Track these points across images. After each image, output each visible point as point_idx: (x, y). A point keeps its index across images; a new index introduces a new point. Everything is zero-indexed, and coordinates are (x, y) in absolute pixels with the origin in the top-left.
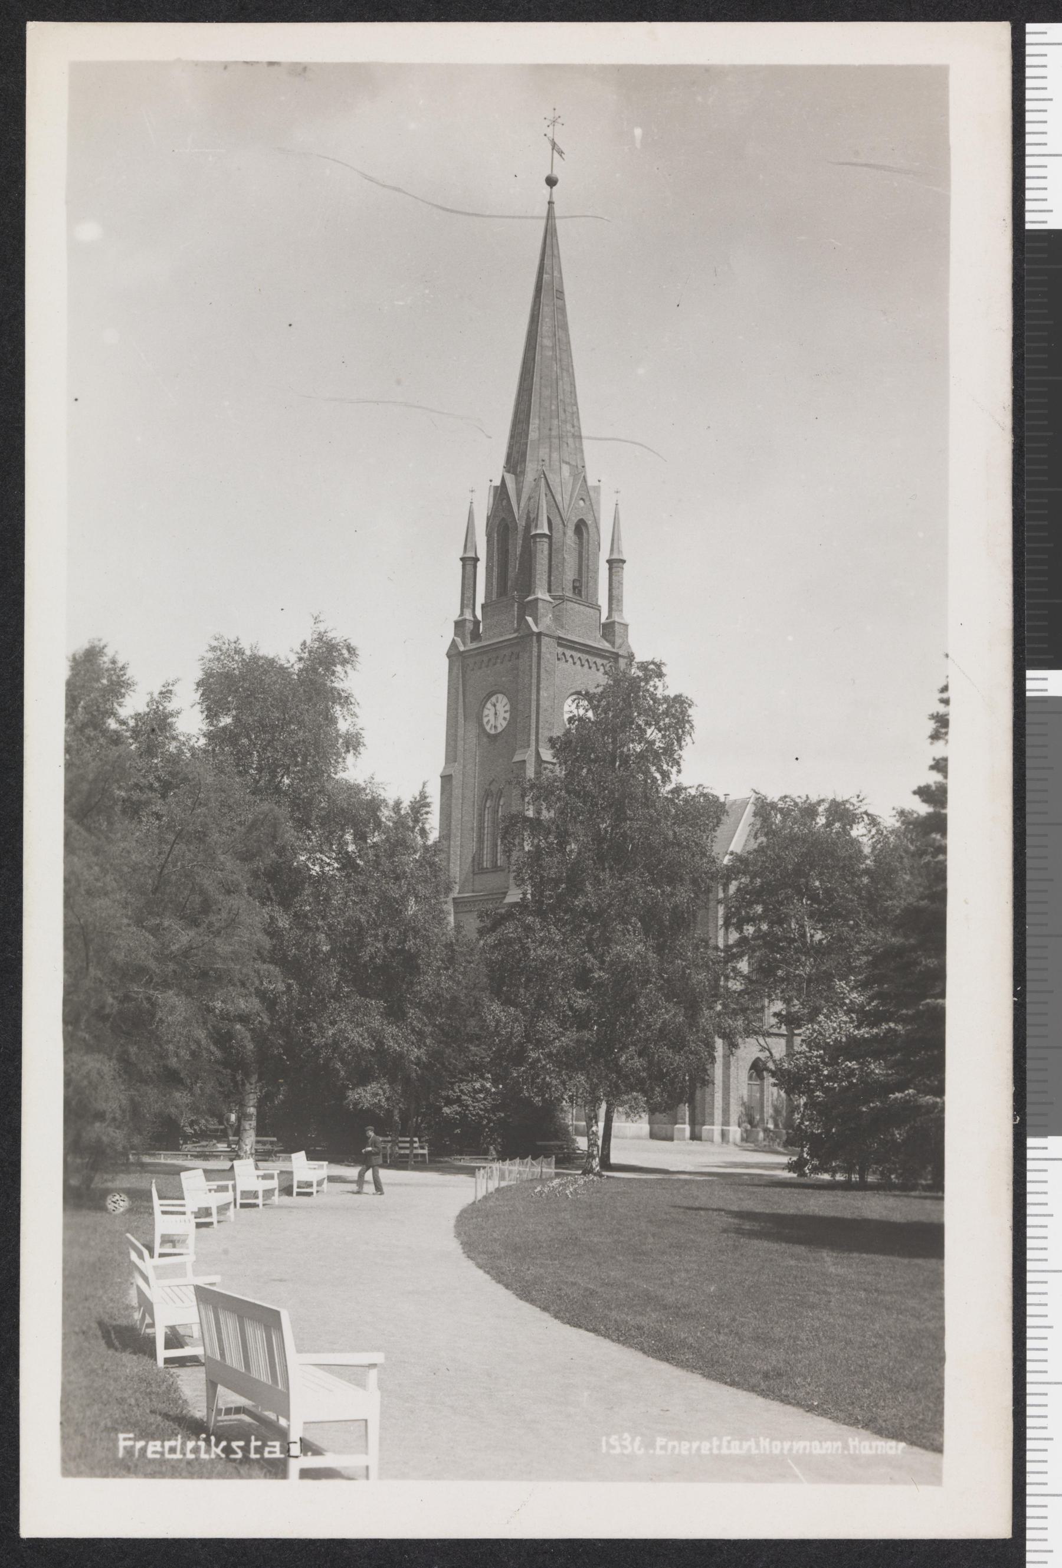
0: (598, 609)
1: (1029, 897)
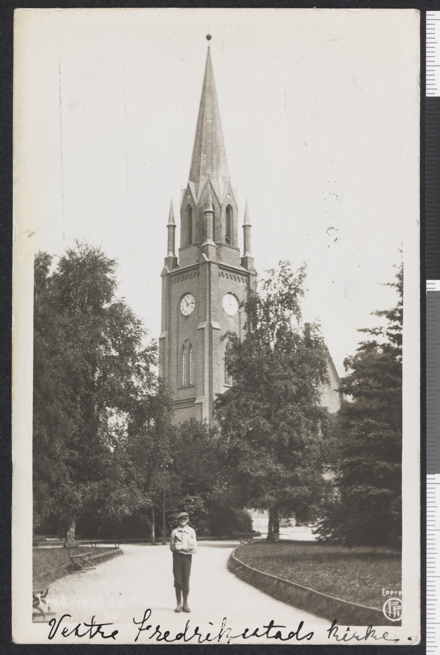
0: (238, 250)
1: (428, 374)
